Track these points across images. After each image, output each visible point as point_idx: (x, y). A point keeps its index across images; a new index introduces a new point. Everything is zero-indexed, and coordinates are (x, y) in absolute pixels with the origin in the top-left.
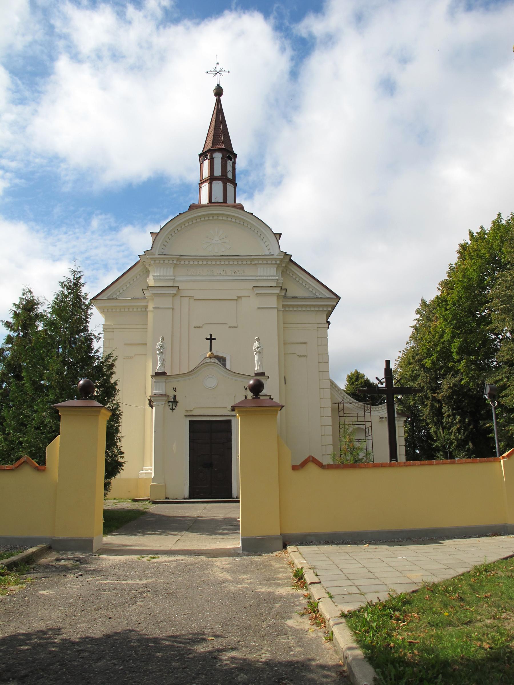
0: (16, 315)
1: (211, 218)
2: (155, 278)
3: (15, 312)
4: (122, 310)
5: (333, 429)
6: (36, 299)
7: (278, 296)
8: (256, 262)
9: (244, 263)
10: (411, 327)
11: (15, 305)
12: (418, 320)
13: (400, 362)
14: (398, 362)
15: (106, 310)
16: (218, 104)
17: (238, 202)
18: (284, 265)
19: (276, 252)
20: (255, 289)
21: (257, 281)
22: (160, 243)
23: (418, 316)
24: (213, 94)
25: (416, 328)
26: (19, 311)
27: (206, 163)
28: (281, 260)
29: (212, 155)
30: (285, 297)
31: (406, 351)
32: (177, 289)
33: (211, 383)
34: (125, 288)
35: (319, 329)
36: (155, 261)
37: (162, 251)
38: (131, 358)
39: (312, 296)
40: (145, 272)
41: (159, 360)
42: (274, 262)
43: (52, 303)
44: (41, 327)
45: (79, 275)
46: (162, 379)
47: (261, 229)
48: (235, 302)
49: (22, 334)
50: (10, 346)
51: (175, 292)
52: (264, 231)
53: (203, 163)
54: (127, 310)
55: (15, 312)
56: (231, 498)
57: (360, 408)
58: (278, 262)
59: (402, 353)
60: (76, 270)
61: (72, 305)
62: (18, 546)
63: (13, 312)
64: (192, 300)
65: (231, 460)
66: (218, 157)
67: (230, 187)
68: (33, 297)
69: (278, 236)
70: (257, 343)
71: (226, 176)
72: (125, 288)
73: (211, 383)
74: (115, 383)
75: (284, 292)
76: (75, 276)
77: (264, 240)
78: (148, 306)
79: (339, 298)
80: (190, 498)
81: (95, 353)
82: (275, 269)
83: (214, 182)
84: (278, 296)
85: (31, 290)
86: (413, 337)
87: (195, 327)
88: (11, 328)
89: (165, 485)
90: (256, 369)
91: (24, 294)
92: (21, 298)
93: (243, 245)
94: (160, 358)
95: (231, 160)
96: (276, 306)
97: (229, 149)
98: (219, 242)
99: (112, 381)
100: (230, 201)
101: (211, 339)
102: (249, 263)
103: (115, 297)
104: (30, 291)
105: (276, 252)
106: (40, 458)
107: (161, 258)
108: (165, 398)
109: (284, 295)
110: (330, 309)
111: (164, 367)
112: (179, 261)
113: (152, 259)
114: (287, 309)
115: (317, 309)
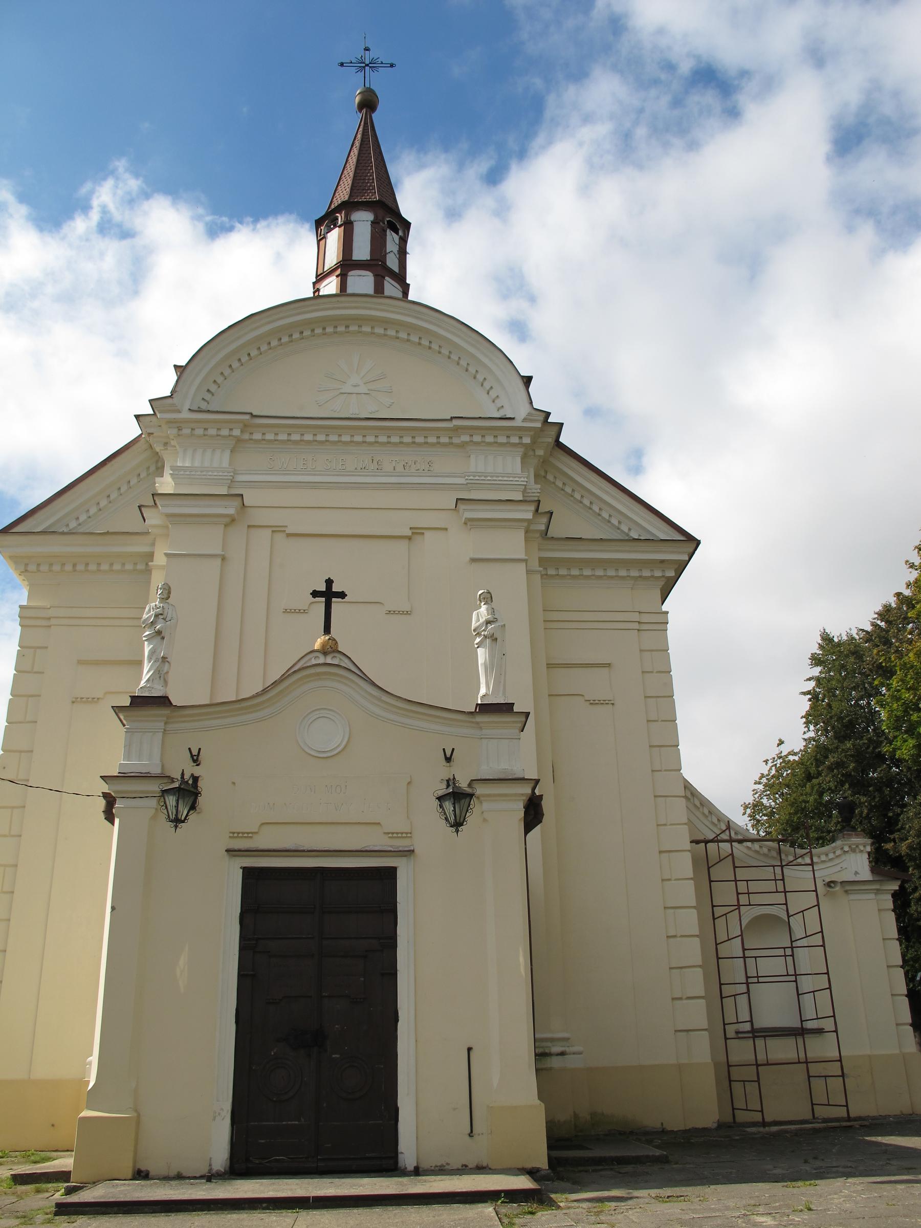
1: (341, 329)
2: (177, 473)
4: (80, 567)
5: (698, 913)
8: (465, 438)
9: (432, 440)
10: (804, 693)
12: (818, 680)
13: (765, 785)
14: (761, 787)
15: (32, 567)
16: (366, 123)
18: (540, 452)
19: (521, 412)
20: (461, 507)
23: (816, 671)
27: (334, 237)
28: (537, 434)
29: (347, 216)
31: (779, 761)
32: (237, 502)
33: (326, 735)
34: (93, 510)
36: (180, 429)
39: (616, 535)
40: (153, 468)
41: (150, 659)
42: (514, 440)
46: (154, 718)
48: (403, 545)
51: (231, 511)
52: (485, 360)
53: (325, 238)
54: (93, 567)
56: (389, 1165)
58: (526, 440)
59: (770, 764)
64: (279, 537)
65: (396, 1020)
66: (363, 221)
70: (484, 608)
72: (93, 510)
73: (326, 735)
75: (545, 520)
77: (487, 385)
78: (153, 553)
79: (693, 543)
80: (241, 1165)
82: (518, 460)
83: (350, 273)
87: (285, 611)
89: (139, 1116)
90: (483, 691)
93: (421, 392)
94: (152, 653)
95: (397, 233)
96: (523, 556)
97: (394, 207)
98: (363, 389)
101: (329, 594)
102: (444, 440)
105: (521, 412)
109: (541, 532)
110: (671, 573)
111: (166, 683)
112: (247, 430)
113: (170, 422)
114: (551, 572)
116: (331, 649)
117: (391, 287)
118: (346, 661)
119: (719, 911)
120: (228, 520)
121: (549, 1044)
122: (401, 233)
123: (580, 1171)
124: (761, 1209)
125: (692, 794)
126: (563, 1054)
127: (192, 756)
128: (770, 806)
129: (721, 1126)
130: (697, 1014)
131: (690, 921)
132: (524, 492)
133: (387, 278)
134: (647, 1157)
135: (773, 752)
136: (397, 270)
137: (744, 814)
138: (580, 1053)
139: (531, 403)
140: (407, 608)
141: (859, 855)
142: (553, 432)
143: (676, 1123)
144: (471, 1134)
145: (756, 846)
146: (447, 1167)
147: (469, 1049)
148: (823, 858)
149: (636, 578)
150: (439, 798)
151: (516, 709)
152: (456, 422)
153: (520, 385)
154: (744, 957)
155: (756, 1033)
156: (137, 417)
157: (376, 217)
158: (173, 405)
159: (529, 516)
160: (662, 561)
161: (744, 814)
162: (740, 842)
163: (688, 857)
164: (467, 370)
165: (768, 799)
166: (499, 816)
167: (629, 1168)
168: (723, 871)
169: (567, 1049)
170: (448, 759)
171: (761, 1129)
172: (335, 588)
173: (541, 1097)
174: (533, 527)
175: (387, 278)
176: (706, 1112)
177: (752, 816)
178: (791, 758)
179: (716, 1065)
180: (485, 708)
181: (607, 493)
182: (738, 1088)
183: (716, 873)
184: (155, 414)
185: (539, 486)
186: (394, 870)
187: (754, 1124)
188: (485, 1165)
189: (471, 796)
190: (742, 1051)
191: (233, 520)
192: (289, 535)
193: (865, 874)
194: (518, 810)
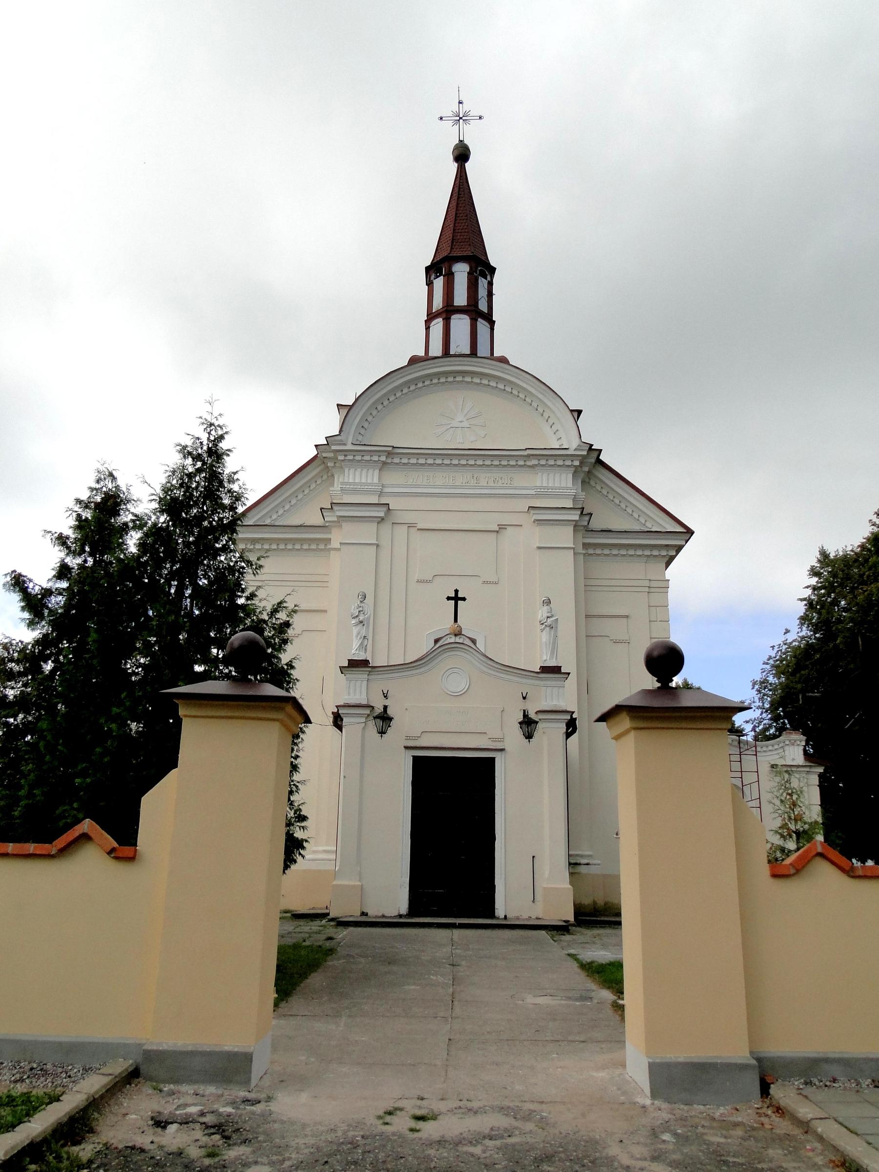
0: (81, 524)
3: (79, 516)
6: (124, 489)
7: (575, 526)
10: (801, 600)
11: (79, 501)
12: (815, 588)
13: (773, 666)
14: (768, 667)
17: (497, 354)
18: (586, 469)
23: (814, 581)
25: (810, 605)
26: (88, 514)
27: (439, 283)
28: (583, 460)
30: (588, 530)
32: (385, 509)
35: (652, 590)
37: (360, 438)
39: (637, 528)
42: (568, 463)
43: (159, 490)
44: (132, 541)
45: (220, 432)
46: (361, 675)
47: (546, 400)
49: (90, 562)
50: (64, 585)
51: (382, 514)
52: (549, 404)
55: (79, 516)
57: (731, 744)
58: (577, 463)
59: (776, 649)
60: (214, 421)
61: (201, 492)
62: (49, 1066)
63: (74, 515)
64: (412, 530)
66: (461, 271)
67: (482, 326)
68: (117, 487)
69: (576, 414)
71: (476, 304)
74: (290, 665)
75: (587, 518)
76: (213, 432)
77: (551, 421)
81: (248, 599)
83: (453, 317)
84: (576, 526)
85: (114, 473)
86: (804, 619)
88: (68, 548)
91: (98, 482)
92: (92, 489)
96: (572, 546)
97: (483, 258)
98: (466, 424)
99: (285, 658)
100: (483, 350)
101: (456, 598)
103: (268, 522)
104: (111, 475)
106: (124, 832)
107: (357, 451)
108: (367, 711)
109: (584, 522)
112: (390, 457)
115: (647, 553)
117: (482, 325)
122: (489, 278)
126: (588, 864)
133: (479, 319)
135: (778, 639)
141: (796, 748)
142: (595, 454)
144: (533, 901)
148: (764, 749)
150: (520, 723)
158: (341, 440)
159: (577, 518)
160: (667, 546)
166: (550, 732)
169: (590, 862)
170: (524, 698)
173: (571, 883)
175: (479, 319)
177: (759, 691)
178: (794, 644)
180: (545, 670)
186: (494, 759)
189: (537, 722)
193: (800, 759)
194: (563, 727)
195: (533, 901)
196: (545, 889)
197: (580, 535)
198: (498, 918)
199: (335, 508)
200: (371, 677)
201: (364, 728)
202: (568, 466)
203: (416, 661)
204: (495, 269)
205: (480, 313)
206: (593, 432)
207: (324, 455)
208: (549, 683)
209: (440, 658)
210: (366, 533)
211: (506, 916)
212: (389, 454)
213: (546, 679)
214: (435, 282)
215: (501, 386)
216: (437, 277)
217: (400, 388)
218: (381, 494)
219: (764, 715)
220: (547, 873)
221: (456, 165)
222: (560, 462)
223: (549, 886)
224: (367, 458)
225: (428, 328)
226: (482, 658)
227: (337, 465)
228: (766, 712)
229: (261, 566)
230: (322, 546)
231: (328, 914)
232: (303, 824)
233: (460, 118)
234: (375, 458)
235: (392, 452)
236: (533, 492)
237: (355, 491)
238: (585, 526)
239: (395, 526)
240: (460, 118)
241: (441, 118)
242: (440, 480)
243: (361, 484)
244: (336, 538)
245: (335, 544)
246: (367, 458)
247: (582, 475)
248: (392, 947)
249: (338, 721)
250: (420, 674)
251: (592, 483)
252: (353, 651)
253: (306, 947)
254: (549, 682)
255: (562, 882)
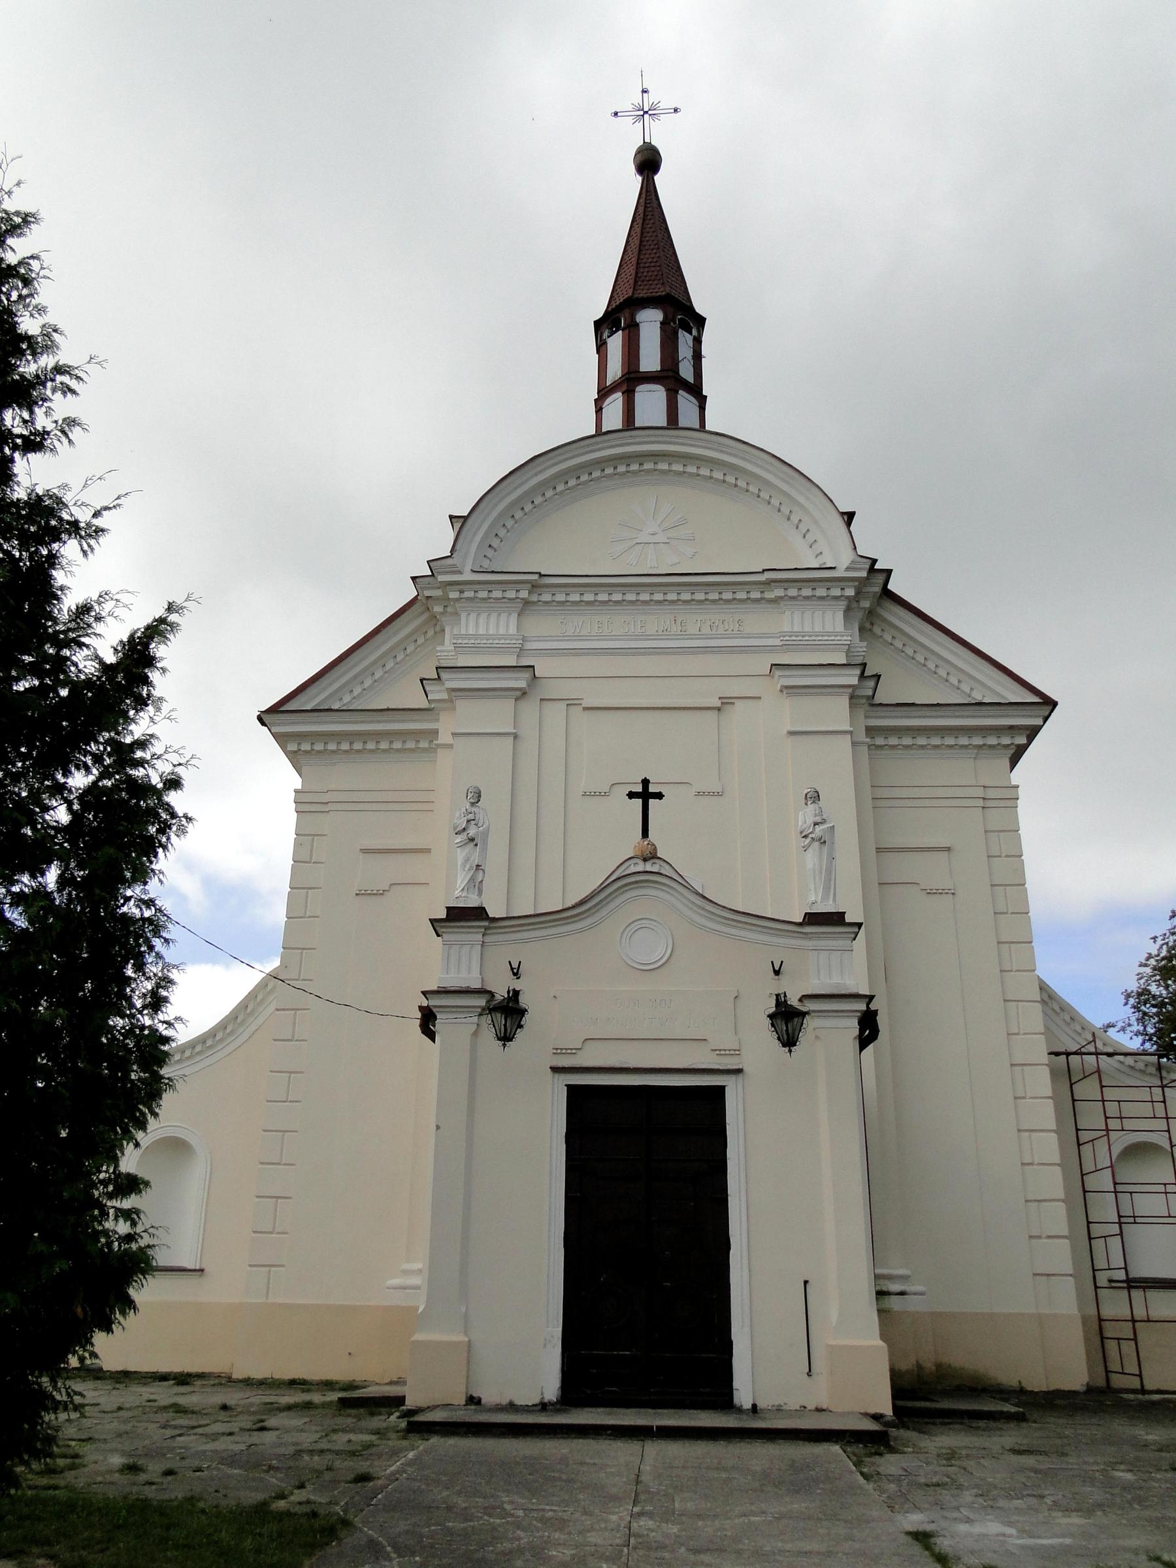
7: (852, 697)
8: (779, 592)
13: (1154, 969)
14: (1148, 970)
18: (866, 604)
21: (786, 647)
22: (478, 538)
24: (632, 168)
27: (616, 343)
28: (861, 584)
30: (872, 704)
32: (527, 675)
33: (650, 947)
35: (989, 804)
38: (381, 894)
42: (836, 592)
47: (793, 493)
51: (522, 684)
52: (801, 499)
58: (850, 592)
59: (1159, 942)
64: (576, 711)
66: (650, 321)
73: (650, 947)
75: (872, 683)
83: (639, 388)
96: (848, 728)
98: (661, 538)
103: (336, 707)
108: (481, 1002)
109: (865, 694)
110: (1022, 740)
112: (536, 592)
115: (977, 741)
116: (651, 856)
117: (685, 402)
118: (667, 867)
119: (1085, 1136)
120: (519, 693)
121: (887, 1282)
122: (694, 332)
123: (927, 1423)
124: (1122, 1467)
125: (1049, 996)
126: (902, 1293)
127: (512, 969)
128: (1161, 996)
129: (1090, 1390)
130: (1060, 1257)
131: (1048, 1147)
132: (848, 652)
133: (680, 392)
134: (1002, 1412)
136: (691, 380)
137: (1126, 1004)
138: (921, 1294)
139: (855, 548)
140: (717, 788)
142: (880, 579)
143: (1037, 1382)
144: (809, 1374)
145: (1130, 1060)
146: (785, 1407)
147: (806, 1282)
149: (980, 747)
150: (771, 1016)
151: (848, 919)
152: (768, 575)
153: (840, 523)
154: (1116, 1192)
155: (1132, 1284)
156: (414, 578)
157: (665, 317)
158: (454, 566)
159: (854, 681)
160: (1011, 727)
161: (1126, 1004)
162: (1110, 1055)
163: (1045, 1073)
164: (779, 511)
165: (1159, 986)
166: (828, 1035)
167: (982, 1424)
168: (1087, 1089)
171: (1140, 1396)
172: (652, 789)
173: (884, 1336)
174: (860, 692)
175: (680, 392)
176: (1075, 1374)
177: (1136, 1008)
179: (1085, 1320)
180: (813, 919)
181: (946, 648)
182: (1111, 1346)
183: (1081, 1090)
184: (433, 575)
185: (865, 644)
187: (1134, 1391)
188: (825, 1407)
189: (803, 1014)
190: (1115, 1305)
191: (524, 693)
192: (585, 709)
194: (852, 1026)
195: (809, 1374)
196: (832, 1349)
197: (861, 714)
198: (740, 1410)
199: (444, 675)
200: (488, 939)
201: (475, 1033)
202: (836, 598)
203: (573, 907)
204: (704, 319)
205: (682, 383)
206: (873, 541)
207: (427, 593)
208: (822, 943)
209: (618, 901)
210: (495, 715)
211: (754, 1406)
212: (534, 587)
213: (818, 936)
214: (609, 341)
215: (718, 475)
216: (612, 334)
217: (551, 483)
218: (521, 652)
219: (1148, 1045)
220: (834, 1317)
221: (640, 179)
222: (821, 592)
223: (841, 1342)
224: (497, 594)
225: (599, 410)
226: (693, 898)
227: (449, 609)
228: (1151, 1039)
229: (99, 531)
230: (424, 744)
231: (401, 1400)
232: (126, 1204)
233: (644, 113)
234: (511, 594)
235: (538, 583)
236: (777, 642)
237: (476, 649)
238: (868, 698)
239: (545, 703)
240: (644, 113)
241: (616, 114)
242: (619, 626)
243: (488, 637)
244: (445, 726)
245: (444, 738)
246: (497, 594)
247: (860, 614)
248: (489, 1511)
249: (428, 1020)
250: (581, 931)
251: (877, 630)
252: (457, 893)
253: (283, 1516)
254: (823, 943)
255: (867, 1336)
